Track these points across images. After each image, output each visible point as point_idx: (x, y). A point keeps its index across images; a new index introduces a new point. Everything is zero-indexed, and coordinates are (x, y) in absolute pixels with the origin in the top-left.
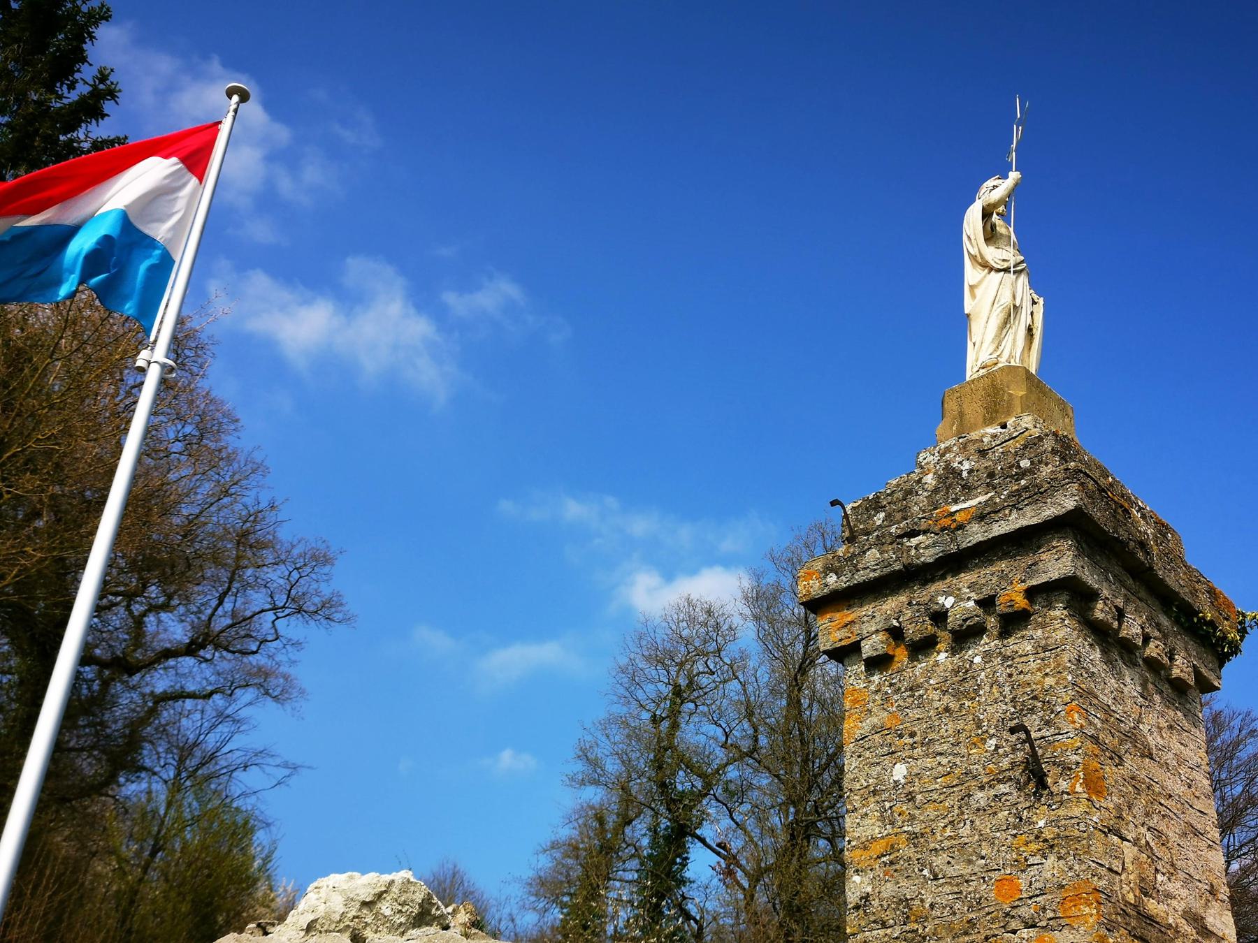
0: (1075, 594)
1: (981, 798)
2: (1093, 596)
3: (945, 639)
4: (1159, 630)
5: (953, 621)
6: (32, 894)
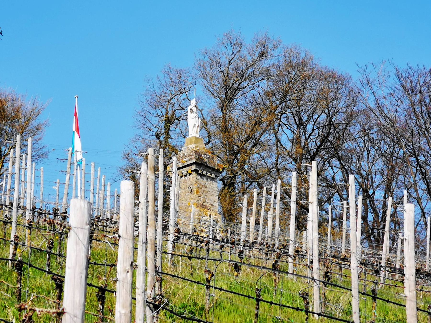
0: (196, 171)
1: (187, 194)
3: (184, 176)
5: (184, 174)
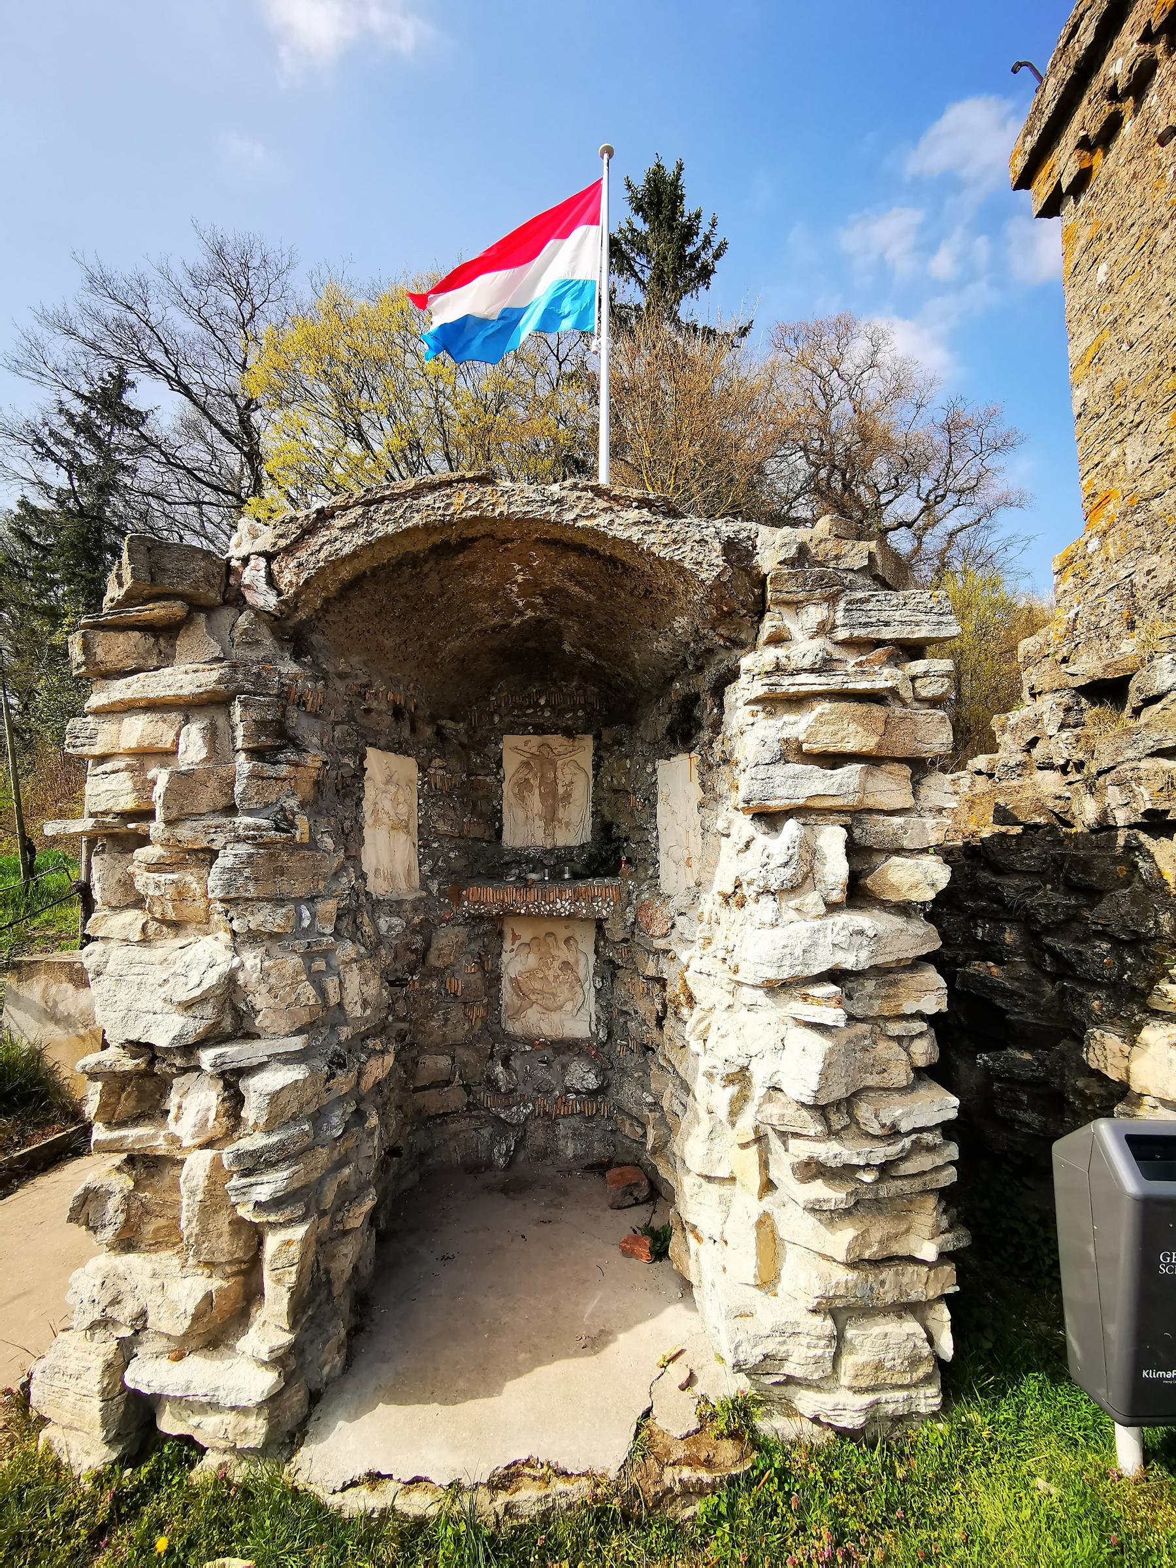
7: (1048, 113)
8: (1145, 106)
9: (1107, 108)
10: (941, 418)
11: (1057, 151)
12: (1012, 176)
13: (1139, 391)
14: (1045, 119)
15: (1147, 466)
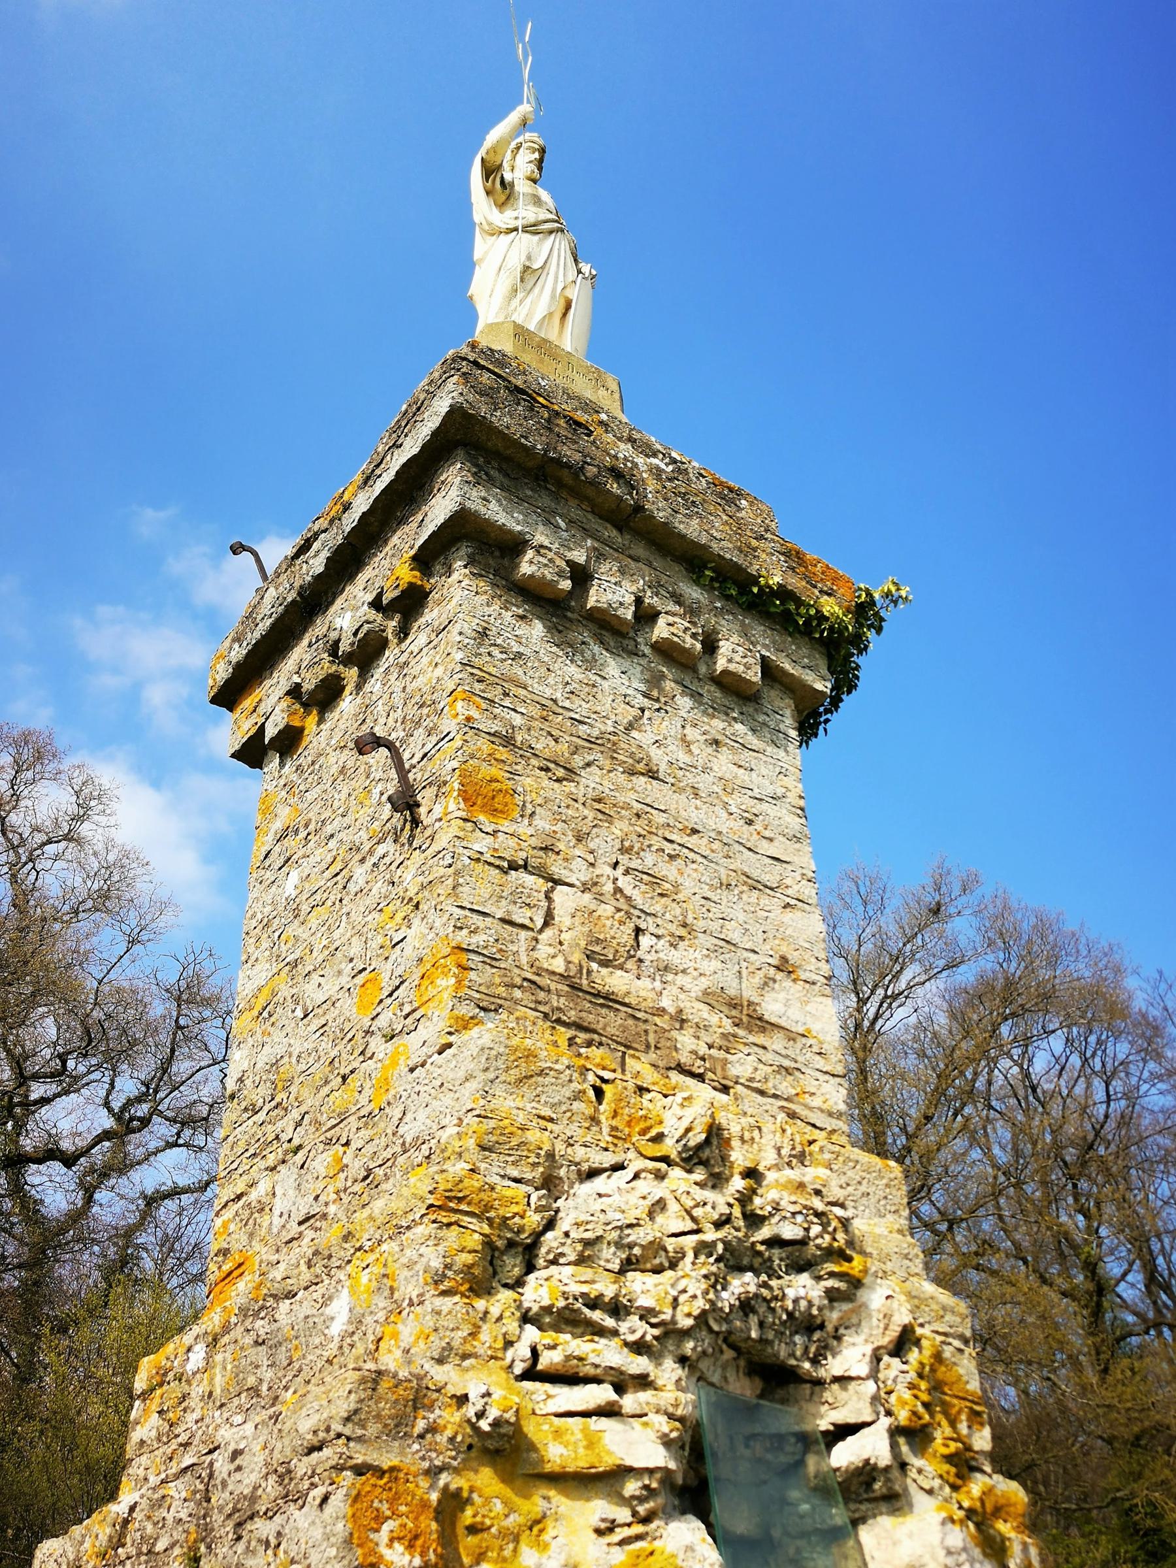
0: (495, 552)
2: (514, 546)
4: (679, 603)
6: (621, 1543)
7: (264, 626)
8: (367, 688)
9: (327, 667)
10: (170, 976)
11: (267, 683)
12: (211, 682)
13: (305, 1093)
14: (257, 635)
15: (294, 1229)
